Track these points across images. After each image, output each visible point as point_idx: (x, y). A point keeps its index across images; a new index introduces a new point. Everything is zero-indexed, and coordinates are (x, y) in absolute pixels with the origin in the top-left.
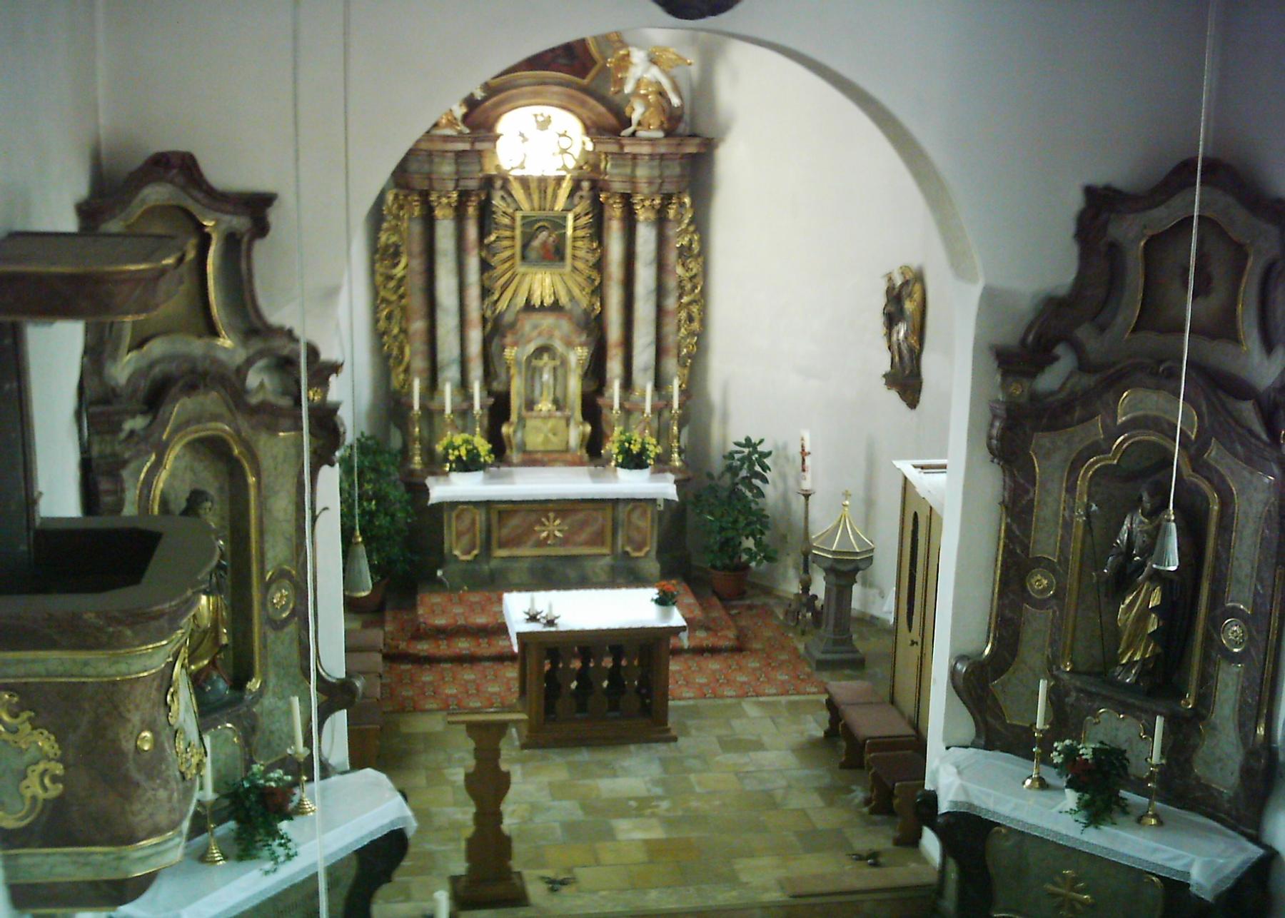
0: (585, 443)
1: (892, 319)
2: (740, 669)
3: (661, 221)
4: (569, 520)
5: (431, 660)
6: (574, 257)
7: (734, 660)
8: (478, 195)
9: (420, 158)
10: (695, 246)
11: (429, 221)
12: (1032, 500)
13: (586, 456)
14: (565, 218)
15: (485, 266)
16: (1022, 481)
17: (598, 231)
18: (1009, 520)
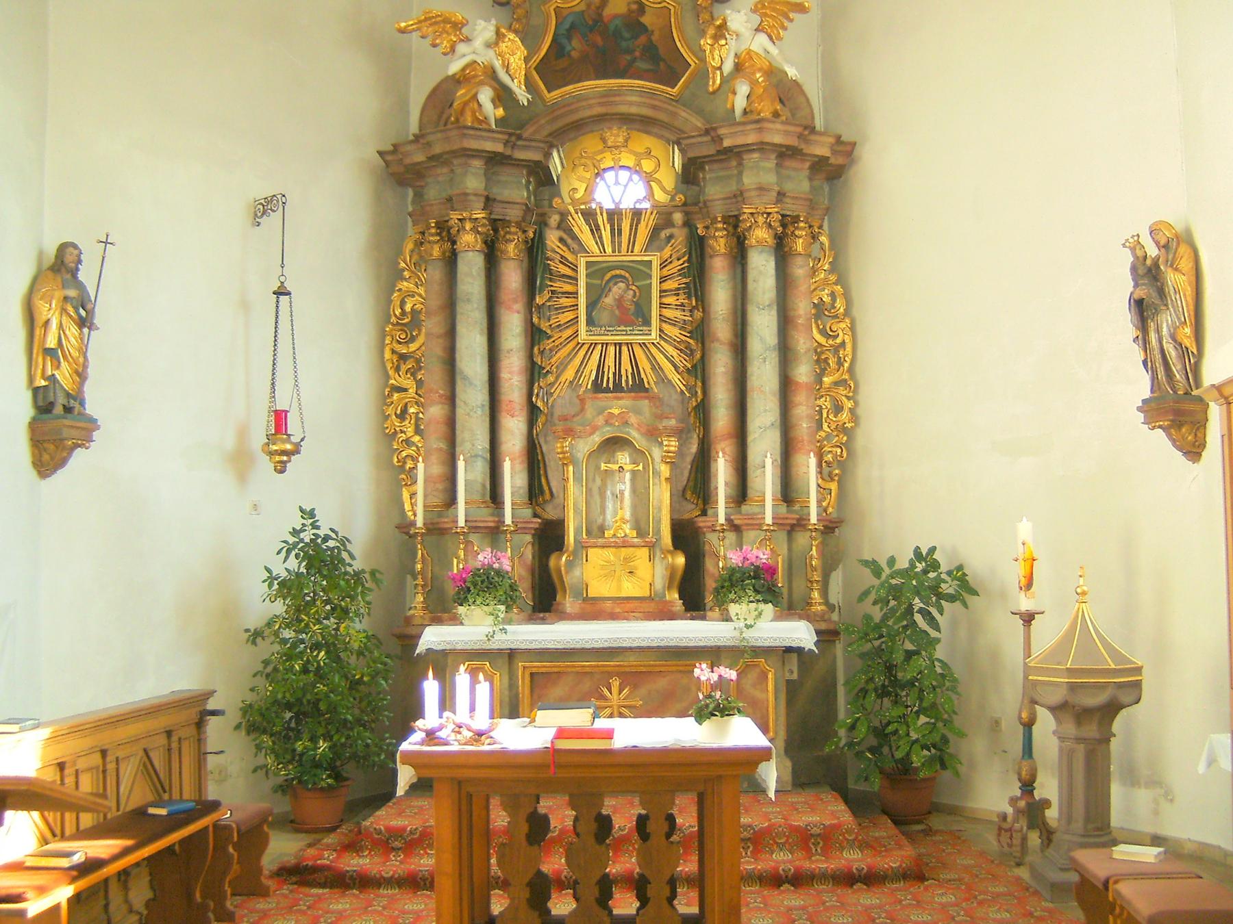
0: (676, 582)
1: (1143, 310)
2: (919, 904)
3: (782, 251)
4: (643, 691)
5: (364, 882)
7: (905, 893)
9: (440, 179)
10: (840, 305)
11: (451, 260)
13: (679, 605)
15: (534, 335)
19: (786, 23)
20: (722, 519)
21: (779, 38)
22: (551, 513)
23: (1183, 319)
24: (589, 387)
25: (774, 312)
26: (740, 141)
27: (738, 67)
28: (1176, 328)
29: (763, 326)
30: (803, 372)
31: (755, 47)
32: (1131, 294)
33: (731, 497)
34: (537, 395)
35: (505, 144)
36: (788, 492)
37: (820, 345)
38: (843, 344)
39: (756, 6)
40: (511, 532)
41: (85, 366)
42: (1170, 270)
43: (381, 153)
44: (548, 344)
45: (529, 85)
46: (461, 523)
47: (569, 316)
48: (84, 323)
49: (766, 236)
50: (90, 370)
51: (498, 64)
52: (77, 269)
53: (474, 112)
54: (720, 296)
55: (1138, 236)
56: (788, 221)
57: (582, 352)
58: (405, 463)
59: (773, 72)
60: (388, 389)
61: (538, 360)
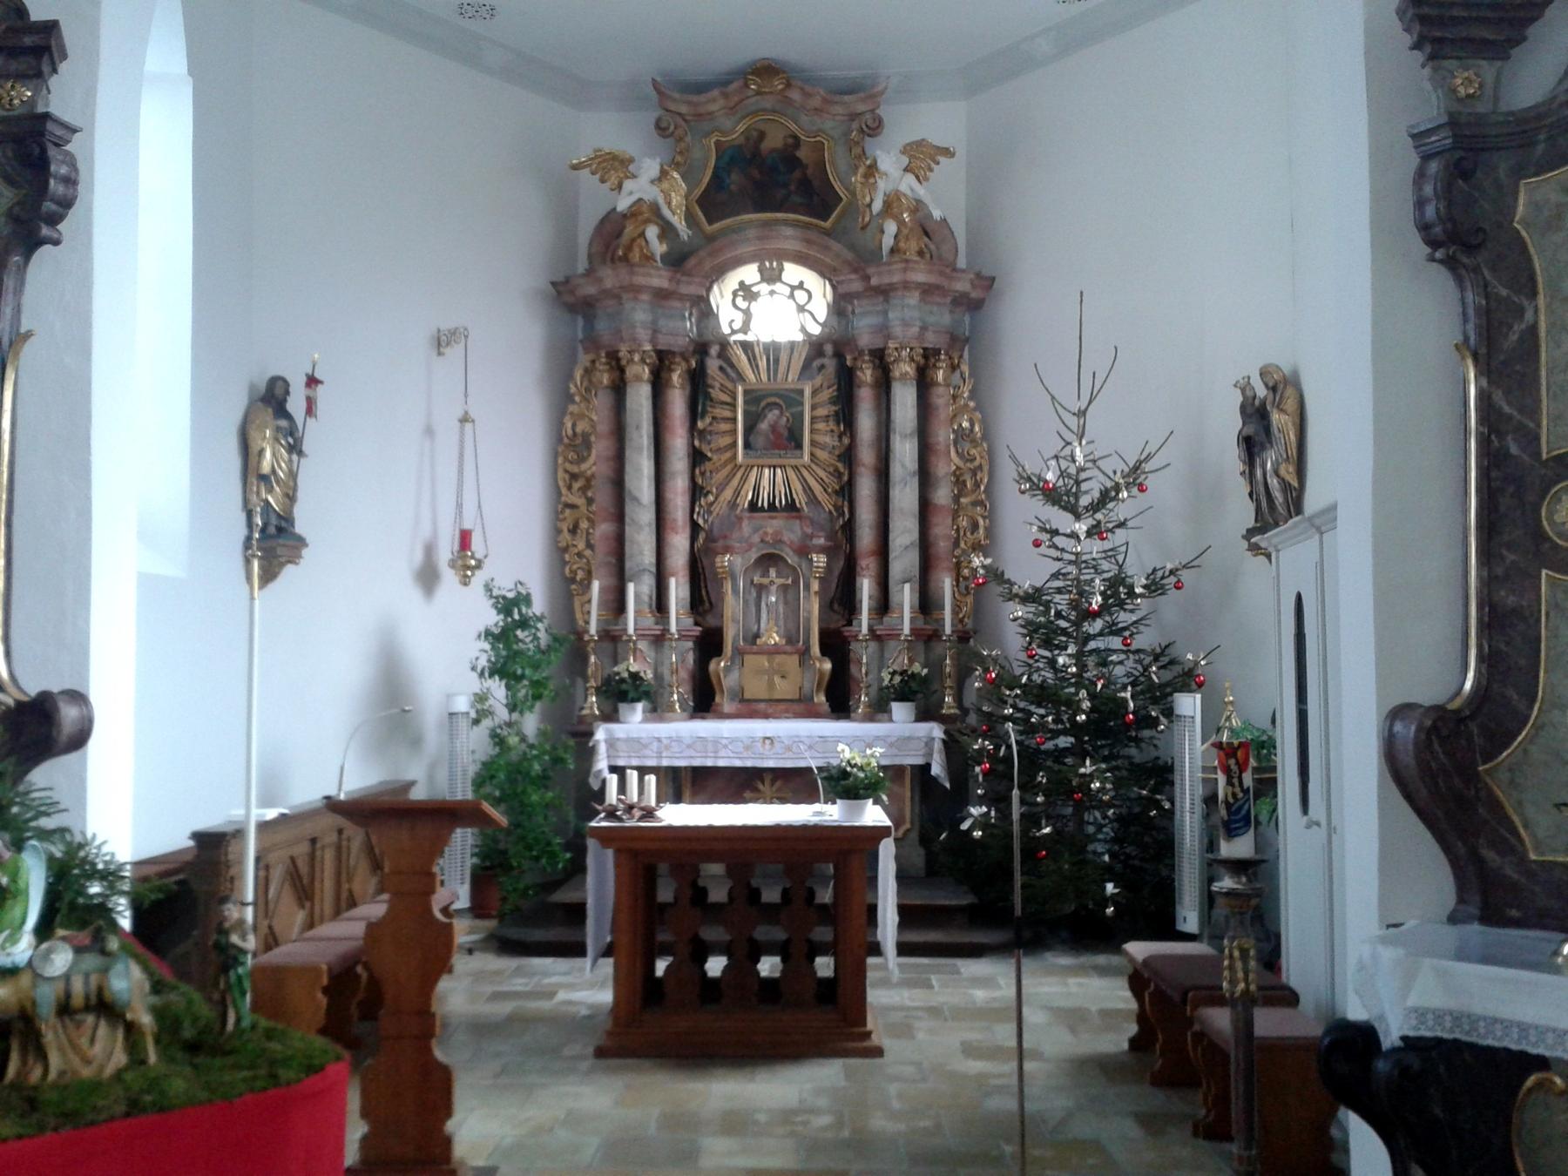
1: (1251, 446)
3: (924, 384)
6: (813, 443)
8: (687, 361)
11: (619, 389)
12: (1533, 330)
13: (826, 707)
14: (801, 392)
15: (697, 458)
16: (1504, 292)
17: (845, 415)
18: (1484, 383)
19: (933, 165)
20: (865, 629)
21: (927, 179)
22: (711, 621)
23: (1285, 456)
24: (746, 505)
25: (915, 442)
26: (886, 280)
27: (888, 205)
28: (1278, 464)
29: (905, 452)
30: (942, 495)
31: (903, 188)
32: (1240, 432)
33: (876, 609)
34: (699, 513)
35: (670, 280)
36: (927, 604)
37: (958, 468)
38: (980, 467)
39: (905, 148)
40: (676, 640)
41: (295, 489)
42: (1275, 411)
43: (553, 284)
44: (708, 466)
45: (690, 218)
46: (631, 630)
47: (727, 440)
48: (296, 448)
49: (908, 369)
50: (300, 494)
51: (661, 201)
52: (285, 400)
53: (642, 250)
54: (866, 423)
55: (1249, 378)
56: (930, 355)
57: (739, 475)
58: (576, 574)
59: (918, 207)
60: (560, 506)
61: (700, 481)
